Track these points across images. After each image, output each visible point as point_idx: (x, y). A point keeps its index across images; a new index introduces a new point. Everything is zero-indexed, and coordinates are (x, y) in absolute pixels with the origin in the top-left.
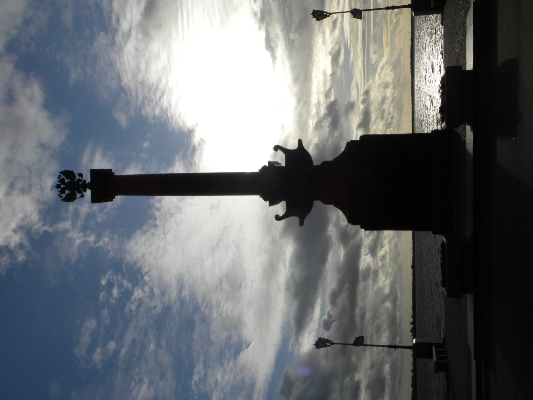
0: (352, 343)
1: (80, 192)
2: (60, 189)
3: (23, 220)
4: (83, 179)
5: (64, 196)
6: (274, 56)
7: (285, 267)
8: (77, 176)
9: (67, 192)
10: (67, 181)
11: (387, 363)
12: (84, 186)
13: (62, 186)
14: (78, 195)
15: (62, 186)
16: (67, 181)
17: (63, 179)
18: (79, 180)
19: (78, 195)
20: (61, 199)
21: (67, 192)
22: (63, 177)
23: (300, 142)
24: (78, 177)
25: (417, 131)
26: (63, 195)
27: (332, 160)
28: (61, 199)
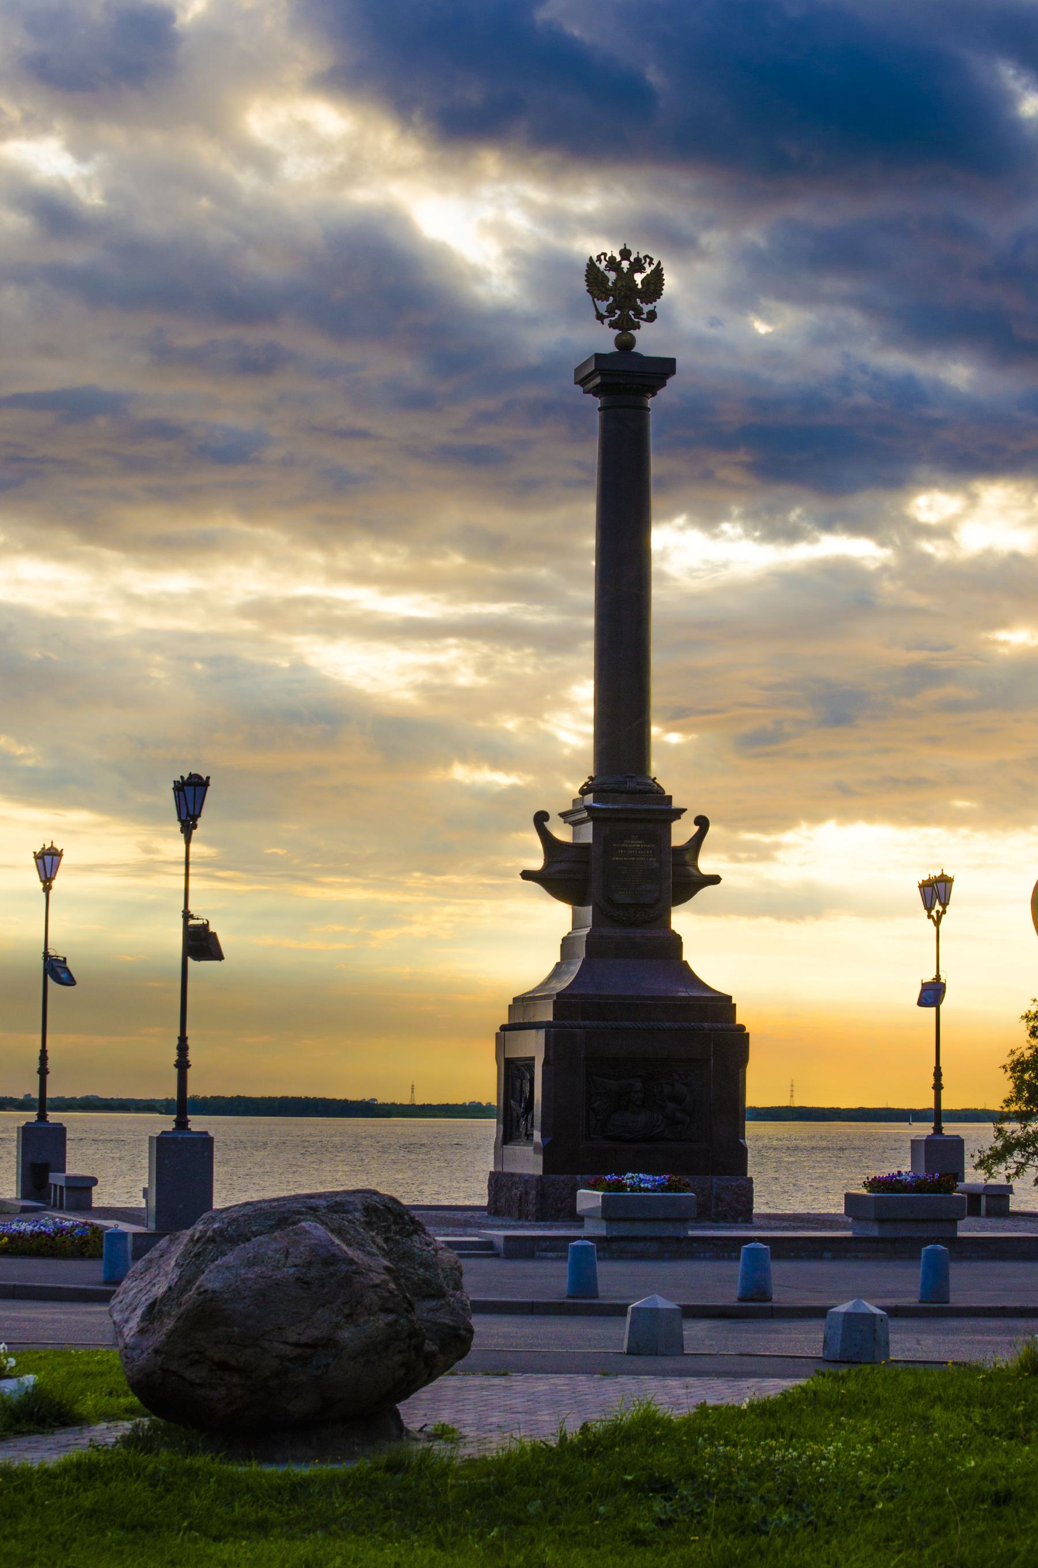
0: (626, 1351)
1: (611, 311)
2: (618, 259)
3: (96, 1503)
4: (642, 323)
5: (602, 266)
6: (788, 846)
7: (386, 918)
8: (650, 307)
9: (612, 276)
10: (639, 278)
11: (575, 835)
12: (625, 326)
13: (625, 265)
14: (603, 306)
15: (625, 265)
16: (639, 278)
17: (641, 270)
18: (639, 312)
19: (603, 306)
20: (595, 259)
21: (612, 276)
22: (649, 270)
23: (715, 880)
24: (646, 308)
25: (752, 1129)
26: (604, 263)
27: (684, 958)
28: (595, 259)
